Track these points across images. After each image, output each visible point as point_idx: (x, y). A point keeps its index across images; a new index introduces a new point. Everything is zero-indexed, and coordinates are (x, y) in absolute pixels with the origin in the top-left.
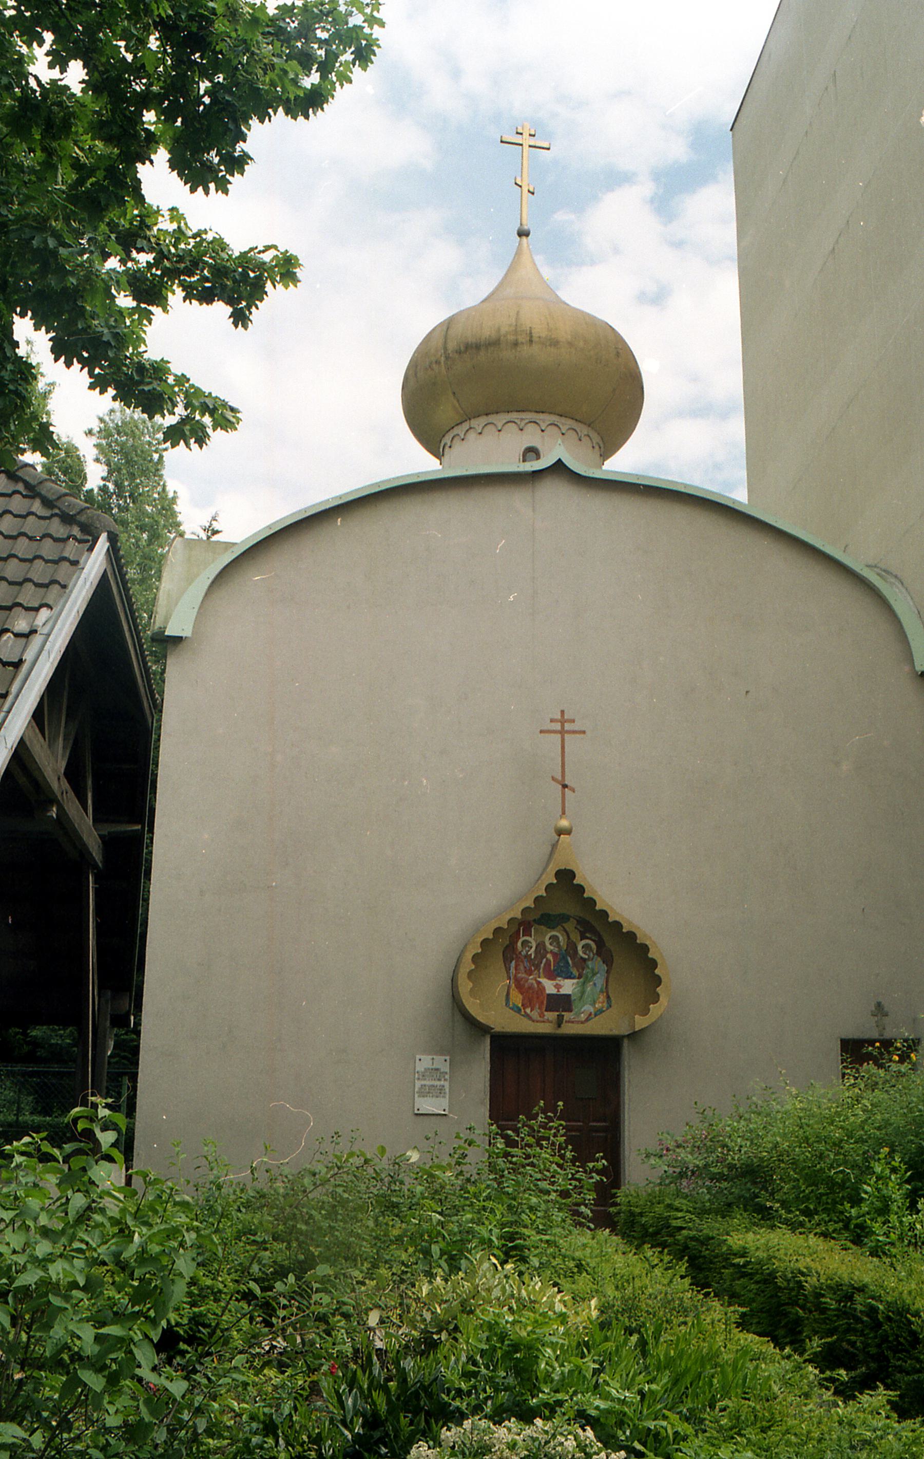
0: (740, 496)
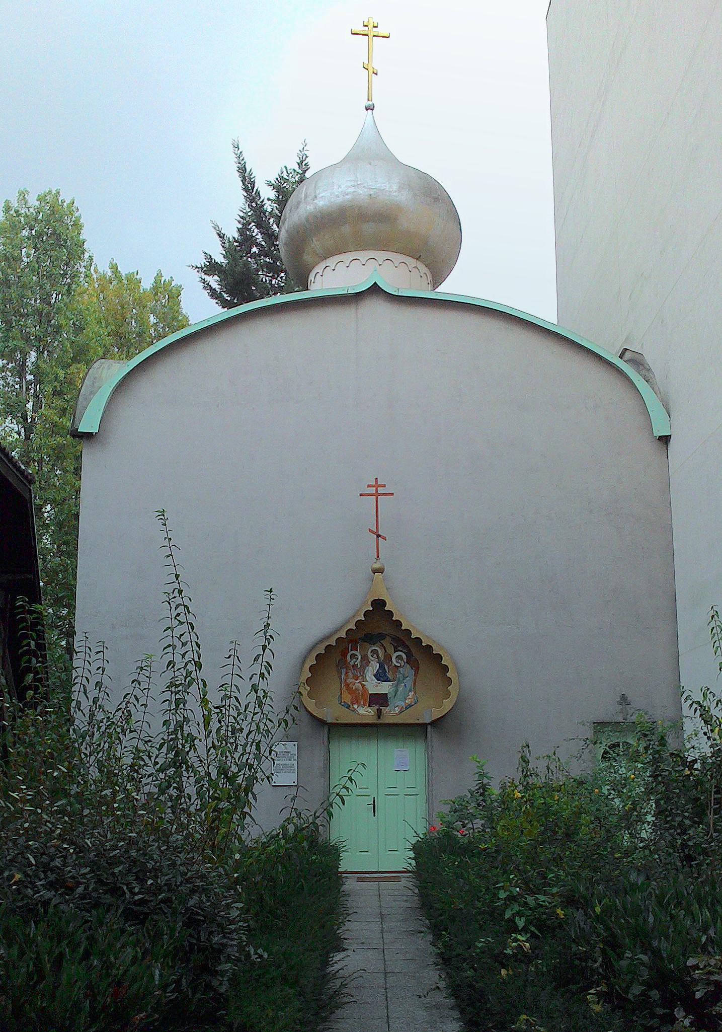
0: (546, 312)
